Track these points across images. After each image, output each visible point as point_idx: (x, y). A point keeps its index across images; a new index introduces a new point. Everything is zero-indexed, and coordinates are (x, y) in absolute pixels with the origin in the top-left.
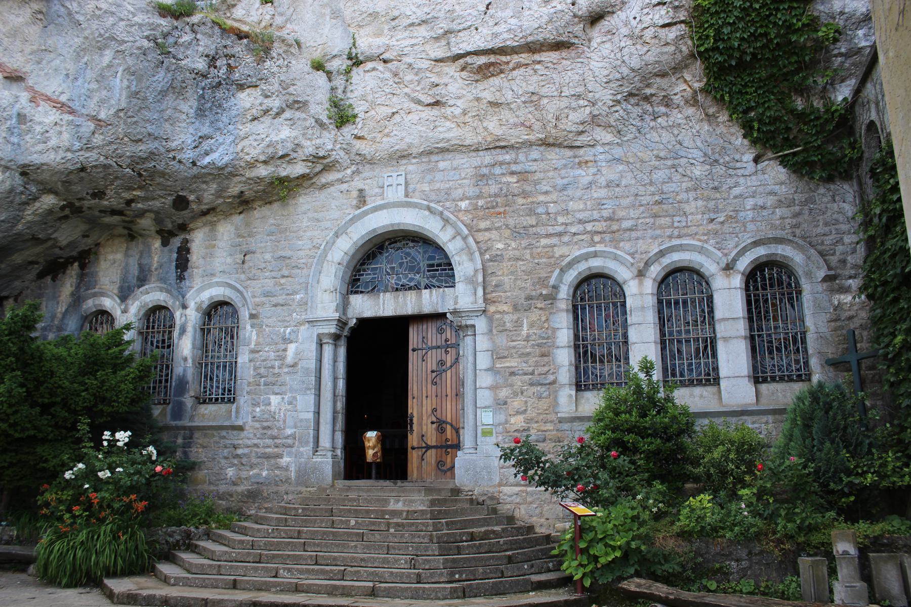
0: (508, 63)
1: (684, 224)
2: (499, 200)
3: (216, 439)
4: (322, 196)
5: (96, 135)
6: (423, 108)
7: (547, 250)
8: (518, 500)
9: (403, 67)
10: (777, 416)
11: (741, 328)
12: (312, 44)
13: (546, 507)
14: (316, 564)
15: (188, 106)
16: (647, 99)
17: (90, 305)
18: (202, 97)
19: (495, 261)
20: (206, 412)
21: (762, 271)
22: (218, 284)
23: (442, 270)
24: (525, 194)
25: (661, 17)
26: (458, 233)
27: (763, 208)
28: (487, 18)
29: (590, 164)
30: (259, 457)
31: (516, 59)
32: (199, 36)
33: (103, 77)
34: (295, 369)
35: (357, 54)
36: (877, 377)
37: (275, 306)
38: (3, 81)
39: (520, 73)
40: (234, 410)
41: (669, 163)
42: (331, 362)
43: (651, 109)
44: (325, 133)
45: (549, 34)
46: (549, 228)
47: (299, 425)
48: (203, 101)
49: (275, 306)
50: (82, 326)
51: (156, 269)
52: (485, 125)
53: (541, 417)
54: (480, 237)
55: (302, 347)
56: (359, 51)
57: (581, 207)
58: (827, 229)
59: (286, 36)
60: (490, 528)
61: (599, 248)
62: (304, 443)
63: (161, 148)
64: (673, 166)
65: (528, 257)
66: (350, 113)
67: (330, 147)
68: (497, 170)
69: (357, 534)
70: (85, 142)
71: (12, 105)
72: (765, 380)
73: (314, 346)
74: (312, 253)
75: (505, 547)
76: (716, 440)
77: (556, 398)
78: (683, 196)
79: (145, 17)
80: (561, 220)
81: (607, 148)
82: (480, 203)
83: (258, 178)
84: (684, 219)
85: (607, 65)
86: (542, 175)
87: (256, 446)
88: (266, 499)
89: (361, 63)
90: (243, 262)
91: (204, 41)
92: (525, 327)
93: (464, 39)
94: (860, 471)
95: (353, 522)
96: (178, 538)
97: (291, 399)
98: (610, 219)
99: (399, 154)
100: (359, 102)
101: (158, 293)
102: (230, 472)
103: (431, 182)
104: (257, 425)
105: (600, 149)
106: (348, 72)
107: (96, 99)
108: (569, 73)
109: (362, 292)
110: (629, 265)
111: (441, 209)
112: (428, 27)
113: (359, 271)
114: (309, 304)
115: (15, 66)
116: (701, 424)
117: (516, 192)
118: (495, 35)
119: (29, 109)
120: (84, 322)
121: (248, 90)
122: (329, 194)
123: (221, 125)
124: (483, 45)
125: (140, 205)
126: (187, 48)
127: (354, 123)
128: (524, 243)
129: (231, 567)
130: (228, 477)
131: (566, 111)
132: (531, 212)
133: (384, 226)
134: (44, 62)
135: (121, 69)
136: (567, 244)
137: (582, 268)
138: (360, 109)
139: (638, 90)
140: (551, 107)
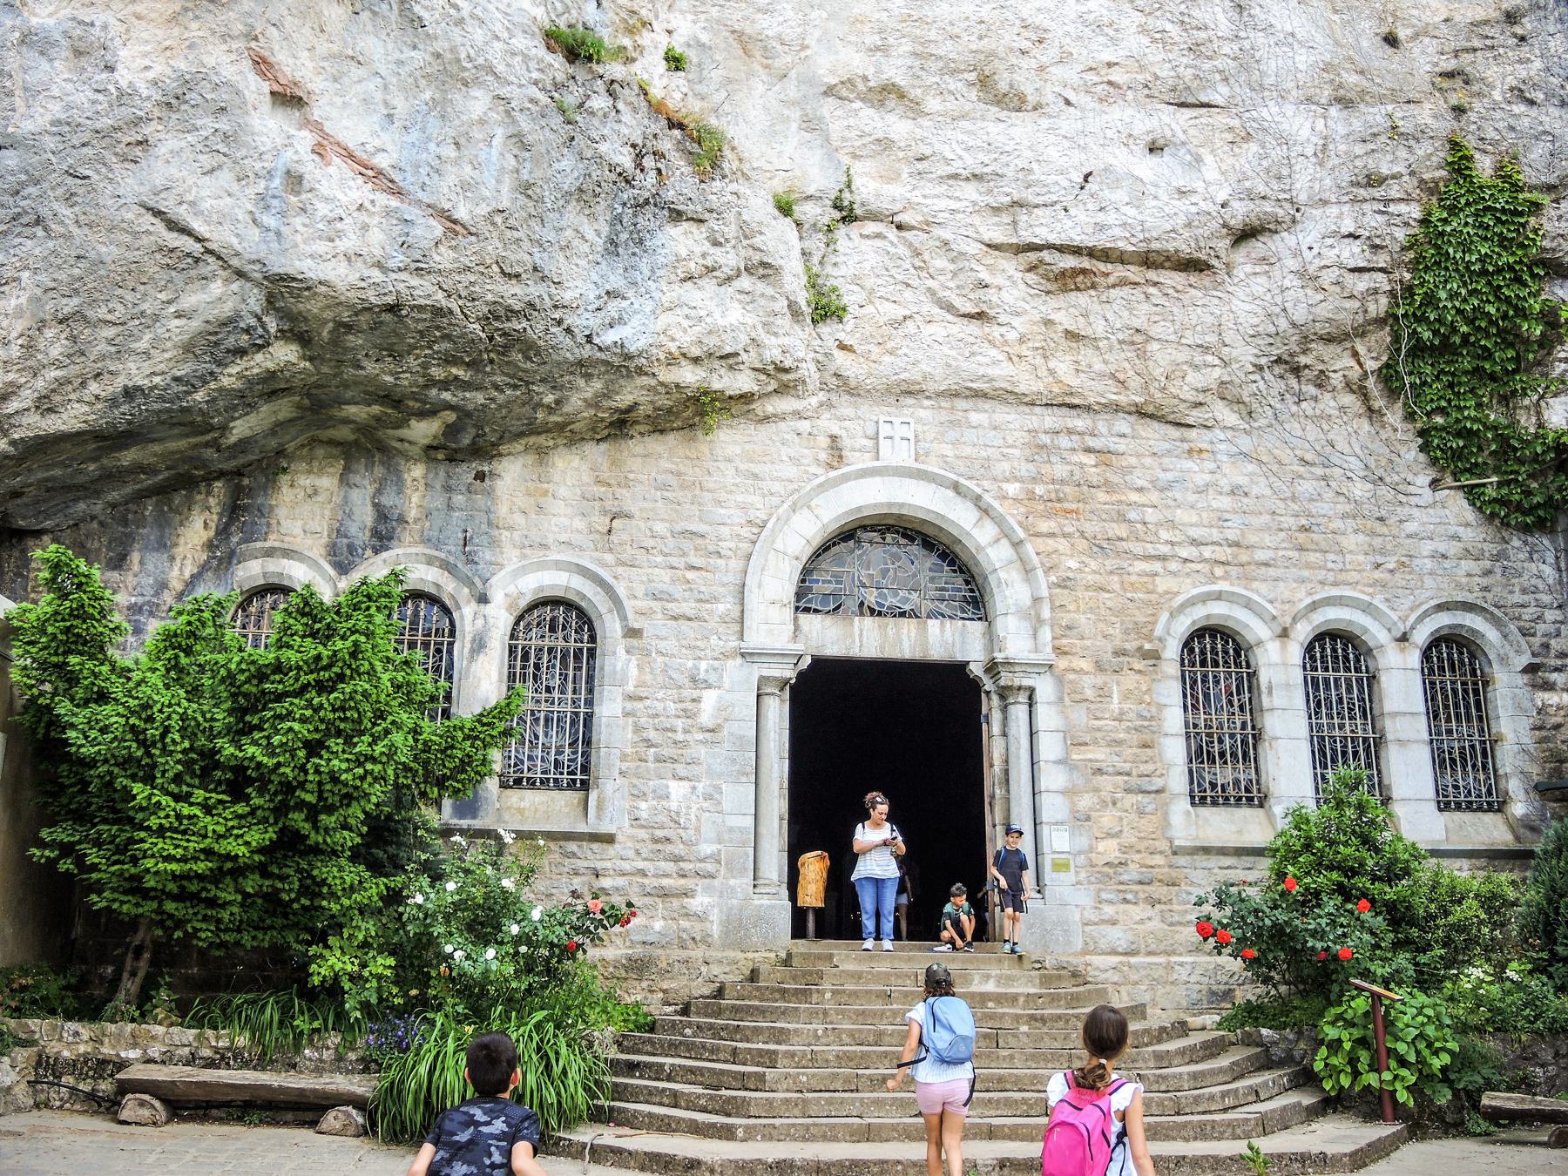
1: (1340, 566)
2: (1067, 489)
4: (766, 431)
5: (442, 249)
7: (1145, 579)
8: (1116, 979)
9: (931, 243)
13: (1161, 990)
15: (594, 231)
16: (1296, 370)
19: (1065, 587)
22: (559, 566)
24: (1109, 487)
25: (1353, 255)
28: (1084, 195)
29: (1205, 455)
31: (1118, 271)
32: (620, 106)
34: (719, 736)
38: (268, 98)
41: (1319, 471)
43: (1296, 387)
45: (1182, 245)
46: (1149, 546)
47: (726, 837)
52: (1051, 365)
53: (1146, 843)
56: (858, 199)
57: (1195, 519)
58: (1526, 597)
61: (1223, 586)
63: (546, 297)
64: (1324, 478)
65: (1117, 587)
68: (1064, 442)
77: (1166, 816)
78: (1337, 524)
79: (531, 44)
80: (1165, 535)
81: (1229, 434)
83: (677, 386)
84: (1339, 558)
86: (1133, 461)
89: (856, 219)
97: (710, 790)
103: (955, 443)
104: (643, 834)
107: (451, 179)
108: (1199, 310)
109: (816, 611)
110: (1268, 618)
111: (979, 491)
112: (983, 187)
116: (1425, 871)
118: (1101, 227)
119: (310, 166)
124: (1078, 239)
131: (1185, 367)
132: (1122, 518)
136: (1174, 574)
138: (851, 297)
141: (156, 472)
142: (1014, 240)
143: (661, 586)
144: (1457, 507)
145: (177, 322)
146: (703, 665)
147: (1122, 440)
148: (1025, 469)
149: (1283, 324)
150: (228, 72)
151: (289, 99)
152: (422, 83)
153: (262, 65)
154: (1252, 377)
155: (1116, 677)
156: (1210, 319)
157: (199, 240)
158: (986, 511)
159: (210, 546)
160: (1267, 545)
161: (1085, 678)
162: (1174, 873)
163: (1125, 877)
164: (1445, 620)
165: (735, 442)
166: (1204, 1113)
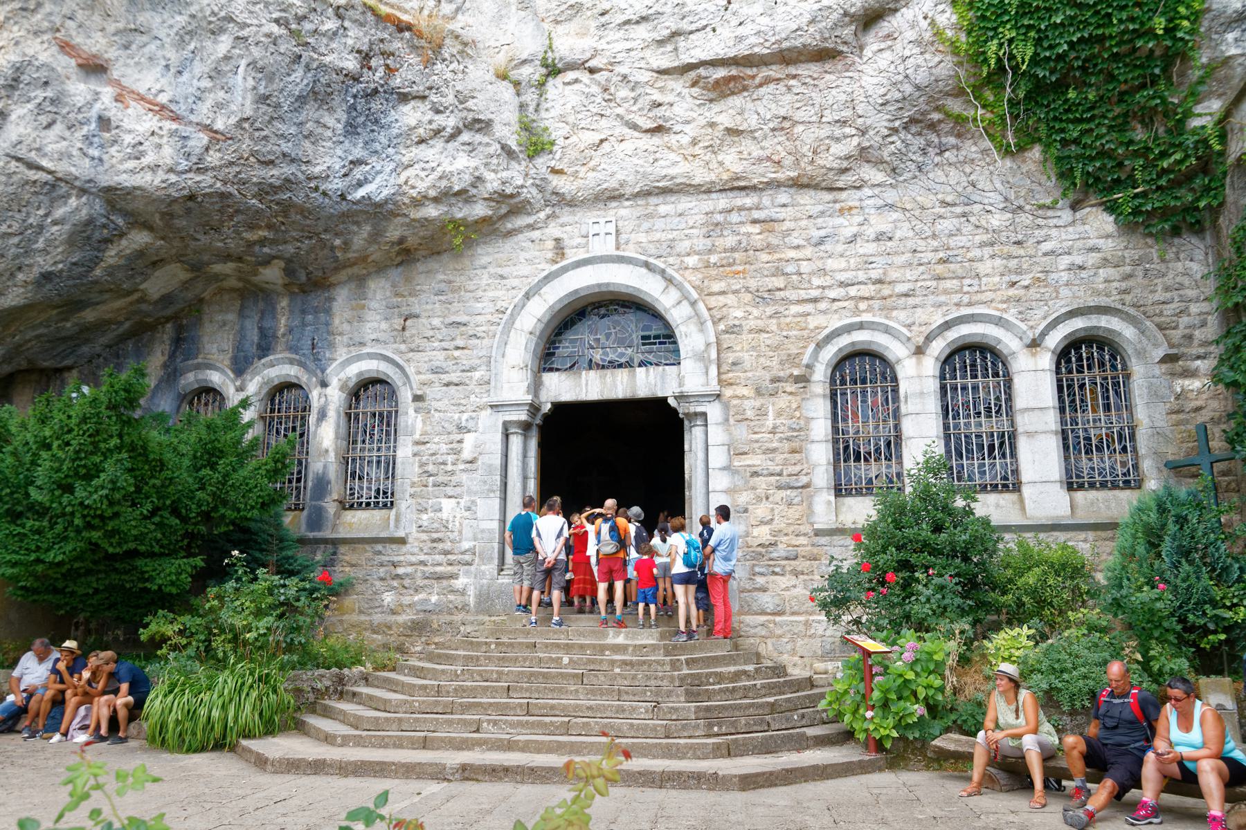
0: (753, 77)
1: (976, 288)
2: (736, 255)
3: (369, 554)
4: (508, 246)
5: (211, 152)
6: (641, 135)
8: (763, 633)
9: (614, 79)
10: (1099, 533)
11: (1051, 420)
12: (493, 44)
13: (800, 642)
14: (528, 714)
15: (335, 120)
16: (932, 126)
17: (190, 380)
18: (353, 107)
19: (733, 333)
20: (355, 520)
21: (1078, 349)
22: (371, 356)
23: (660, 343)
24: (769, 248)
26: (685, 296)
27: (1081, 268)
28: (728, 15)
29: (854, 211)
30: (427, 578)
31: (765, 72)
32: (347, 24)
33: (219, 72)
35: (554, 60)
36: (1233, 485)
37: (447, 385)
38: (76, 70)
39: (769, 90)
40: (392, 517)
41: (959, 210)
42: (520, 457)
43: (936, 140)
44: (514, 164)
45: (811, 38)
48: (354, 114)
49: (447, 385)
50: (179, 407)
51: (284, 335)
52: (720, 158)
53: (792, 528)
54: (712, 301)
55: (485, 437)
57: (843, 265)
58: (1168, 295)
59: (460, 31)
60: (741, 668)
61: (866, 317)
62: (485, 559)
63: (300, 174)
64: (964, 215)
65: (774, 328)
66: (545, 139)
67: (520, 182)
68: (734, 217)
69: (575, 676)
70: (195, 160)
71: (90, 105)
72: (1081, 487)
73: (499, 437)
74: (495, 318)
75: (763, 692)
76: (1029, 561)
77: (810, 506)
78: (976, 253)
80: (816, 281)
81: (877, 190)
82: (713, 259)
83: (426, 219)
84: (976, 282)
85: (885, 81)
87: (423, 563)
88: (437, 631)
89: (560, 72)
90: (404, 329)
91: (354, 32)
92: (771, 415)
93: (697, 43)
94: (1228, 604)
95: (566, 660)
96: (328, 683)
97: (469, 504)
98: (880, 281)
99: (607, 194)
100: (557, 125)
101: (287, 366)
102: (388, 598)
104: (424, 536)
105: (867, 191)
106: (542, 85)
107: (209, 103)
108: (834, 92)
109: (557, 370)
110: (904, 340)
111: (662, 266)
113: (554, 342)
114: (493, 383)
115: (94, 50)
116: (1010, 542)
117: (759, 245)
118: (740, 39)
119: (114, 111)
120: (182, 402)
121: (412, 102)
122: (517, 244)
123: (377, 146)
125: (266, 250)
126: (331, 39)
127: (551, 152)
128: (770, 310)
129: (417, 720)
130: (386, 603)
133: (588, 287)
134: (134, 47)
135: (243, 63)
136: (824, 312)
137: (844, 341)
138: (558, 132)
139: (922, 114)
140: (807, 136)
141: (120, 323)
142: (676, 64)
143: (438, 363)
144: (1098, 224)
145: (56, 228)
146: (465, 416)
147: (783, 209)
148: (702, 243)
149: (908, 89)
150: (44, 57)
151: (94, 68)
152: (187, 38)
153: (66, 47)
154: (890, 139)
155: (772, 399)
156: (843, 97)
157: (50, 172)
158: (670, 281)
159: (165, 366)
160: (905, 278)
161: (746, 402)
162: (815, 550)
163: (775, 555)
164: (1078, 324)
165: (488, 254)
166: (690, 737)
